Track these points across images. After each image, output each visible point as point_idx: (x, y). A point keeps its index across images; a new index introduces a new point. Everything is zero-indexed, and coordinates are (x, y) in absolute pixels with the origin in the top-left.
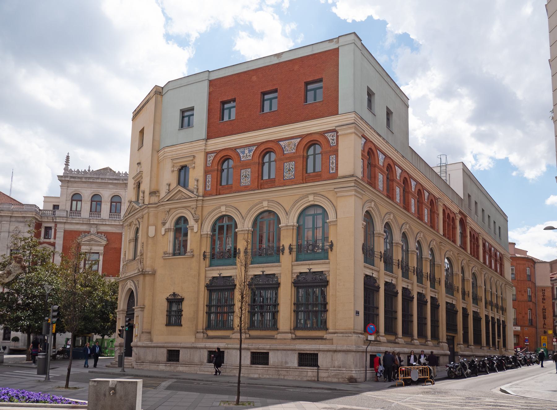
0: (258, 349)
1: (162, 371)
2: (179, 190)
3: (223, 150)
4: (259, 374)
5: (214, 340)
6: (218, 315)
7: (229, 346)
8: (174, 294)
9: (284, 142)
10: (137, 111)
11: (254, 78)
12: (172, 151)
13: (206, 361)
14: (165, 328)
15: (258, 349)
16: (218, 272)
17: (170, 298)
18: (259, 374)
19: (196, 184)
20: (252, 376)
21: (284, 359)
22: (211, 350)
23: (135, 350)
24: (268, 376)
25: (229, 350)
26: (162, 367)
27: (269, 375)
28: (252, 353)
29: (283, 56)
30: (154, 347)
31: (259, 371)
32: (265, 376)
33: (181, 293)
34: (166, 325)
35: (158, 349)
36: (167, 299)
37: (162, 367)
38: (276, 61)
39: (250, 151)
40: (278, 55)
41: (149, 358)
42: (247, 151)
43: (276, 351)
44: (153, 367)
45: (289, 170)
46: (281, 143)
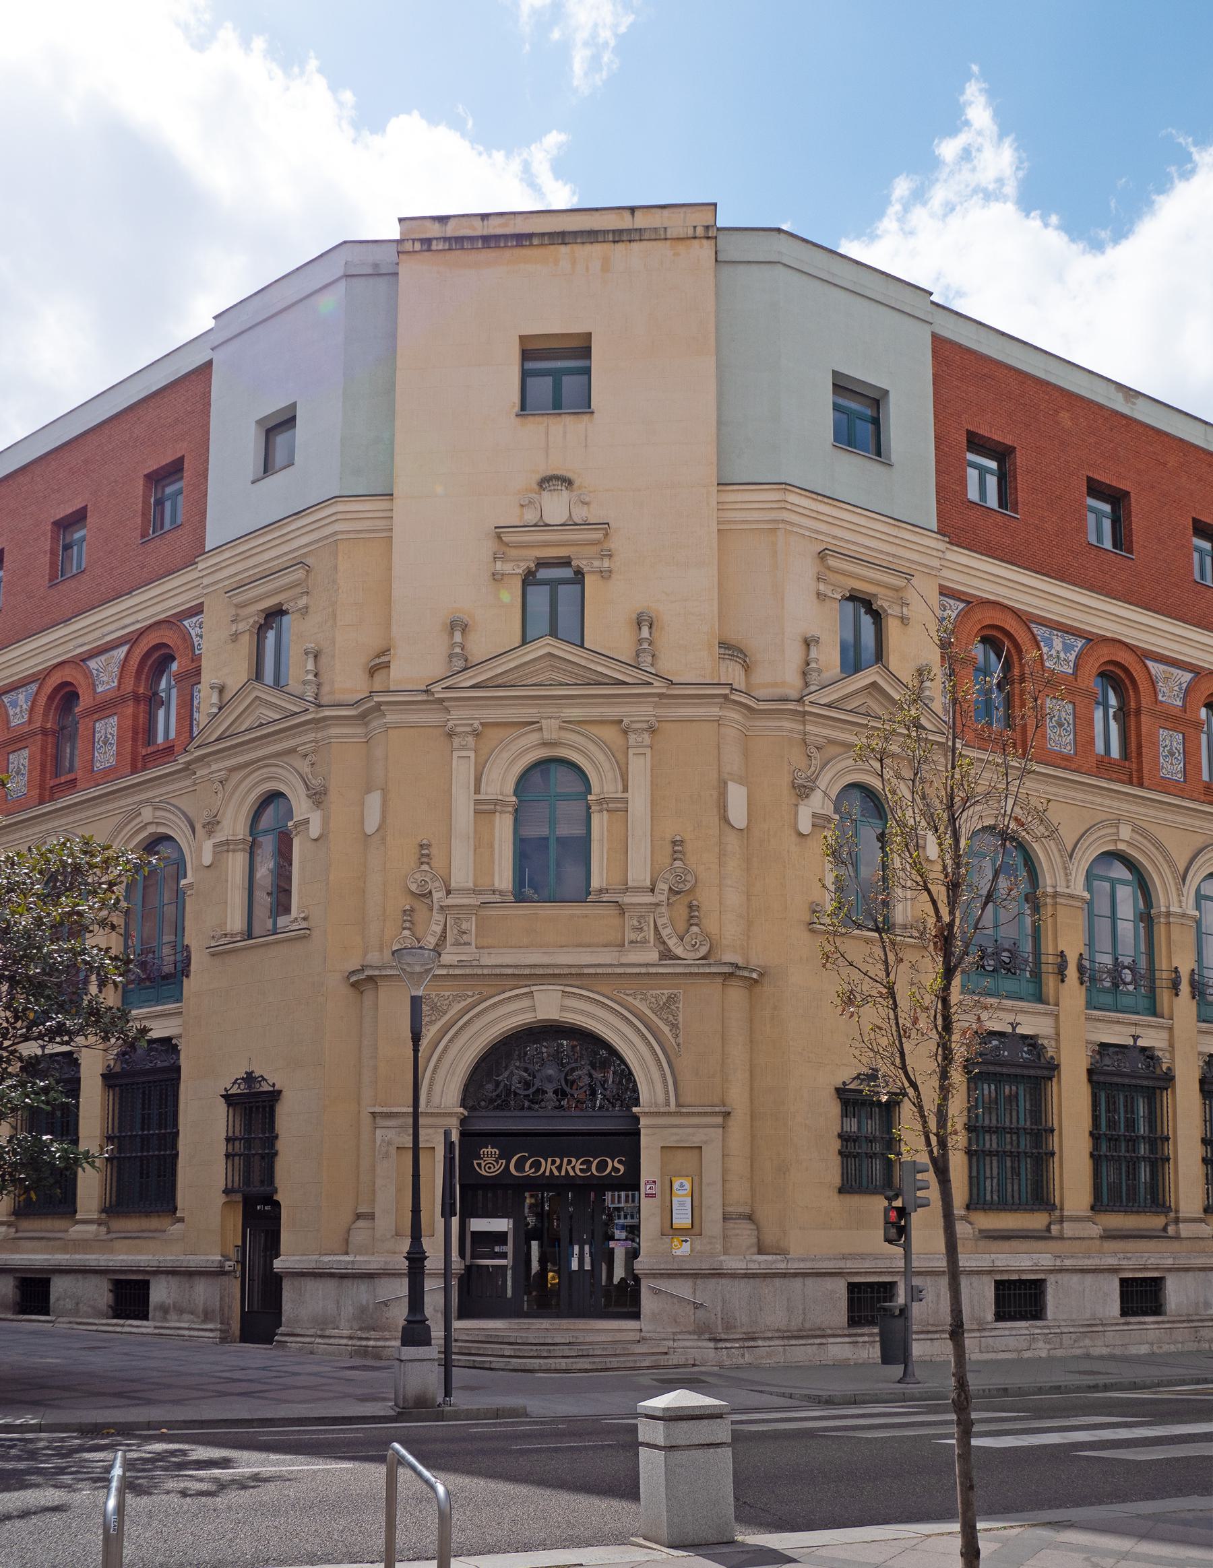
0: (1146, 1269)
1: (841, 1366)
2: (874, 685)
3: (989, 602)
4: (1152, 1344)
5: (1015, 1244)
6: (1012, 1164)
7: (1068, 1262)
8: (249, 1078)
9: (98, 659)
10: (493, 228)
11: (1065, 417)
12: (816, 516)
13: (990, 1315)
14: (836, 1202)
15: (1146, 1269)
16: (1010, 1017)
17: (235, 1090)
18: (1152, 1344)
19: (310, 665)
20: (1133, 1350)
21: (1083, 1300)
22: (1005, 1277)
23: (299, 1304)
24: (1172, 1348)
25: (1059, 1276)
26: (839, 1350)
27: (1175, 1343)
28: (1122, 1280)
29: (1140, 402)
30: (795, 1275)
31: (1151, 1335)
32: (1167, 1348)
33: (274, 1077)
34: (841, 1191)
35: (810, 1281)
36: (227, 1097)
37: (839, 1350)
38: (1119, 404)
39: (1067, 648)
40: (1130, 394)
41: (775, 1317)
42: (1058, 644)
43: (1182, 1274)
44: (802, 1353)
45: (1172, 754)
46: (92, 664)
